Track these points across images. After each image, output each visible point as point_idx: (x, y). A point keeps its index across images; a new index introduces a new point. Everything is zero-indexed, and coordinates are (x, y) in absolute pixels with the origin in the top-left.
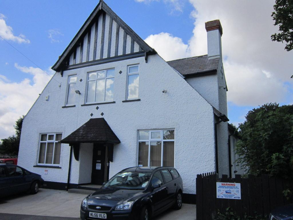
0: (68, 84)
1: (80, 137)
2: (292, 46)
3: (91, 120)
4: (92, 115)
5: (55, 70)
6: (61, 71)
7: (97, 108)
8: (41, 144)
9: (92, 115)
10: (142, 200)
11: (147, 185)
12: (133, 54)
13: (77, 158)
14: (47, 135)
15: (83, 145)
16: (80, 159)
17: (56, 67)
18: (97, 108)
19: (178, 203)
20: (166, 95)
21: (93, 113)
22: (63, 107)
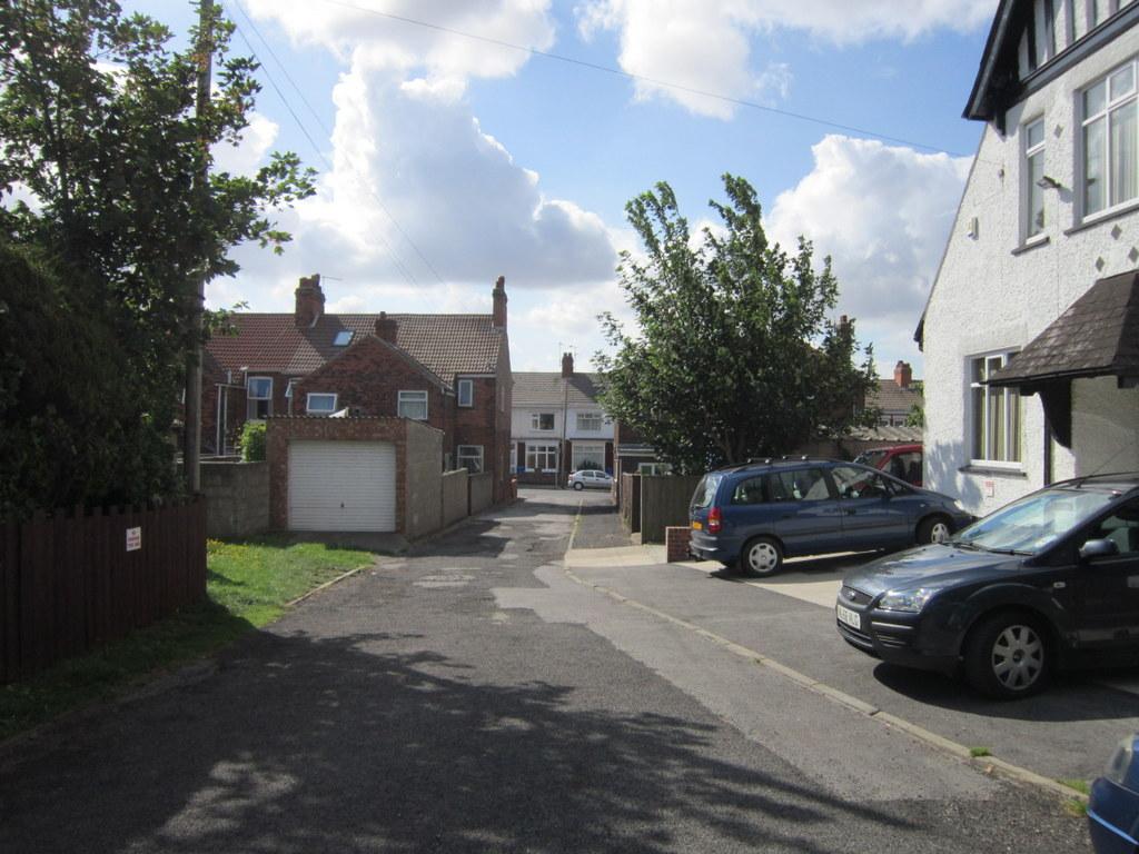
0: (1026, 156)
1: (1043, 360)
2: (44, 10)
3: (1100, 282)
4: (1100, 264)
5: (975, 118)
6: (996, 119)
7: (1116, 233)
8: (470, 478)
9: (1100, 264)
10: (1063, 605)
11: (1057, 541)
12: (1121, 16)
13: (1066, 442)
14: (983, 359)
15: (1081, 386)
16: (1074, 441)
17: (974, 111)
18: (1116, 233)
19: (267, 777)
20: (998, 180)
21: (1102, 256)
22: (1017, 253)
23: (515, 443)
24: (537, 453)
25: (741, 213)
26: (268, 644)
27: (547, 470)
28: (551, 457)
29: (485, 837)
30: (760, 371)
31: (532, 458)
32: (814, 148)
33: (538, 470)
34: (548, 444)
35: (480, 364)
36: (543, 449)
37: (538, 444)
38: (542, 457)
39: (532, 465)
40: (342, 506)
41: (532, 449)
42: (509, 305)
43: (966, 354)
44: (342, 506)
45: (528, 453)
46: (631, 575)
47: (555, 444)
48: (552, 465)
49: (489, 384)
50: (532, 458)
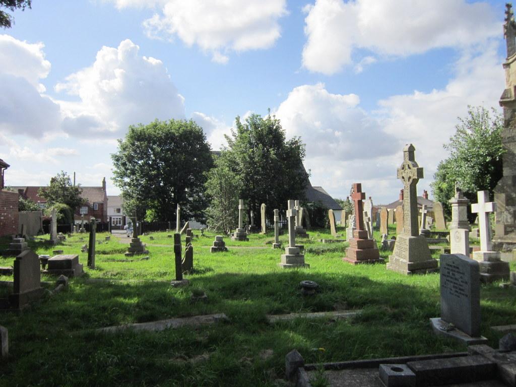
14: (267, 233)
23: (109, 217)
24: (115, 220)
25: (513, 50)
26: (73, 260)
27: (118, 225)
28: (120, 221)
29: (200, 276)
30: (340, 134)
31: (114, 221)
32: (104, 47)
33: (116, 225)
34: (119, 217)
35: (100, 200)
36: (117, 219)
37: (115, 217)
38: (117, 221)
39: (114, 224)
40: (483, 102)
41: (114, 219)
42: (106, 184)
43: (145, 121)
44: (483, 102)
45: (112, 220)
46: (290, 202)
47: (121, 217)
48: (120, 223)
49: (102, 204)
50: (114, 221)
